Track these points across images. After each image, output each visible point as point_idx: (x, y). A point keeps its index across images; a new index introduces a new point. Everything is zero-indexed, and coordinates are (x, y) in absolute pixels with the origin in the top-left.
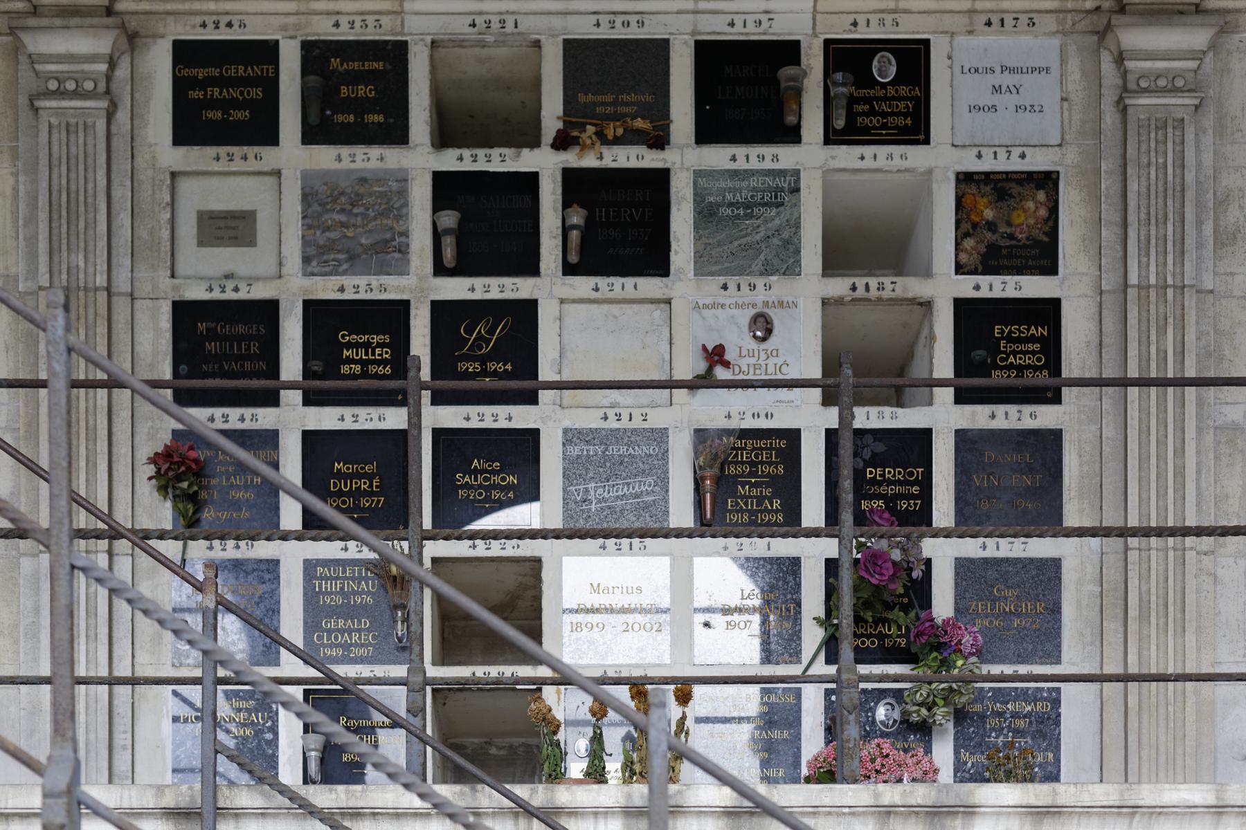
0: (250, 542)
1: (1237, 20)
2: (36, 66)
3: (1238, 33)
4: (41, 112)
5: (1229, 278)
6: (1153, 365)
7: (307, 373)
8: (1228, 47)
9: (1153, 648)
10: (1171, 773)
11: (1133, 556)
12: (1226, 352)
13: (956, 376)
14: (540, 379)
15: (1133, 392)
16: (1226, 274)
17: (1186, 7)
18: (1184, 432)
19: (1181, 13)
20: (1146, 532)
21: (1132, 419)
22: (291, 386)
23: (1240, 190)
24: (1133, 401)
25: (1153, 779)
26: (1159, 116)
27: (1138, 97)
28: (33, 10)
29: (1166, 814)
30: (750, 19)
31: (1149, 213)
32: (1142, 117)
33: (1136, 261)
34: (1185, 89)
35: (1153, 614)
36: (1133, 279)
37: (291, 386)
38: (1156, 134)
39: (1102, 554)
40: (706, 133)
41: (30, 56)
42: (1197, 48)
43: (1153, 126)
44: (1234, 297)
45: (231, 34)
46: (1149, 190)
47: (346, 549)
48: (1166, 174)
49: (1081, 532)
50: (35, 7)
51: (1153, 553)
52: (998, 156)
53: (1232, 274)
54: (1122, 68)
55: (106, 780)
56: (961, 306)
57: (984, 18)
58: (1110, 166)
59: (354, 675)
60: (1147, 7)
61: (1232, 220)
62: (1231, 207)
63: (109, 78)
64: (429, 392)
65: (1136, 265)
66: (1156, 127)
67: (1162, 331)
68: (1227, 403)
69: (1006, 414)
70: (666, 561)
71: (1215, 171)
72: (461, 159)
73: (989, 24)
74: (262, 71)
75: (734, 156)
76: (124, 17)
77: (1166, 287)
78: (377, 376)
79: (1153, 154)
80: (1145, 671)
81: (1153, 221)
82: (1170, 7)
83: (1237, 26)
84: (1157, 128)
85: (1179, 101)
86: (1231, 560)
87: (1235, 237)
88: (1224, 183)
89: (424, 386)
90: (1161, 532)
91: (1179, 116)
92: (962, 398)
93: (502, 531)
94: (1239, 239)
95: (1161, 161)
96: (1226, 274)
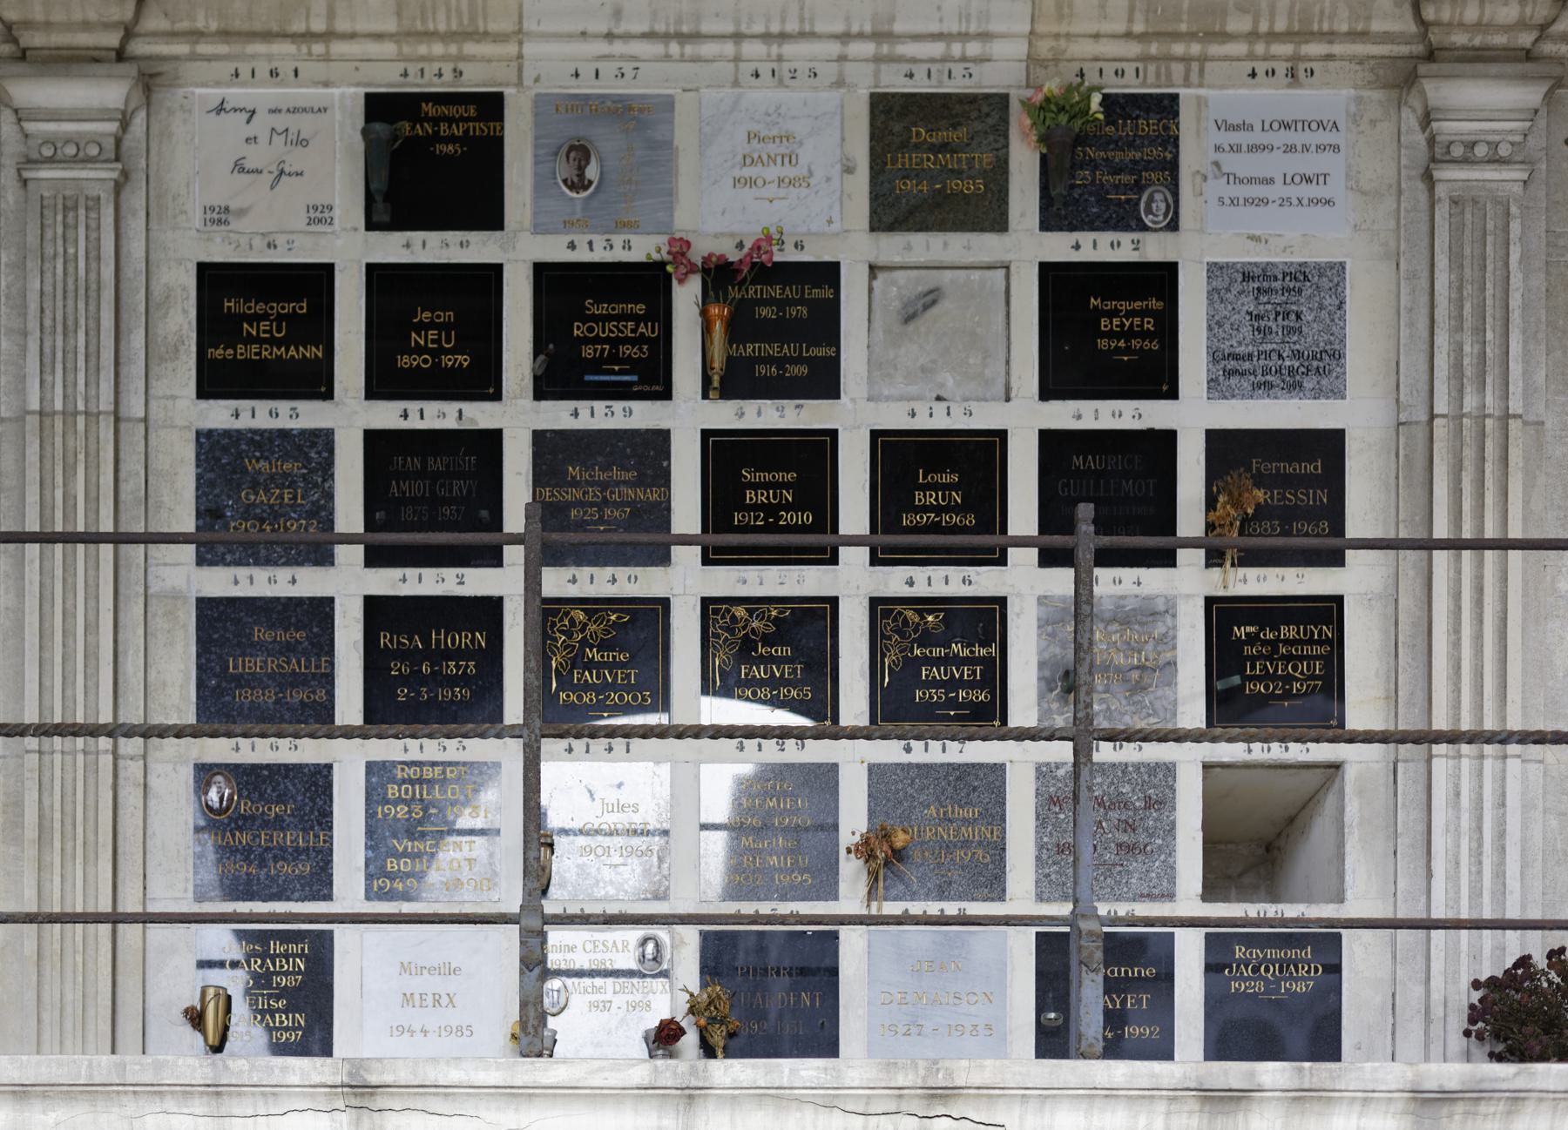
0: (1266, 745)
3: (180, 86)
4: (29, 183)
5: (170, 403)
6: (59, 515)
11: (1440, 767)
12: (165, 499)
13: (1041, 532)
14: (841, 532)
15: (1440, 557)
17: (104, 53)
19: (96, 60)
20: (1453, 738)
21: (31, 583)
22: (686, 540)
23: (184, 289)
24: (32, 561)
25: (57, 1048)
26: (68, 193)
27: (38, 169)
28: (19, 55)
29: (1117, 1096)
30: (1109, 69)
31: (54, 319)
32: (46, 194)
34: (102, 158)
36: (1441, 407)
37: (686, 540)
38: (65, 217)
39: (144, 757)
40: (490, 217)
41: (16, 111)
42: (112, 106)
43: (60, 206)
44: (175, 427)
47: (1250, 751)
48: (76, 268)
49: (1368, 737)
50: (24, 51)
53: (174, 398)
55: (34, 1048)
57: (751, 67)
58: (13, 257)
59: (768, 912)
60: (54, 52)
62: (172, 311)
63: (118, 142)
65: (37, 386)
68: (165, 564)
70: (665, 770)
71: (24, 264)
72: (909, 247)
73: (1253, 75)
74: (489, 128)
75: (572, 242)
77: (76, 413)
78: (789, 529)
79: (60, 242)
81: (59, 329)
83: (177, 78)
84: (65, 208)
85: (92, 174)
86: (169, 767)
87: (177, 350)
88: (163, 281)
90: (1474, 738)
92: (376, 557)
93: (1376, 733)
94: (182, 352)
95: (71, 251)
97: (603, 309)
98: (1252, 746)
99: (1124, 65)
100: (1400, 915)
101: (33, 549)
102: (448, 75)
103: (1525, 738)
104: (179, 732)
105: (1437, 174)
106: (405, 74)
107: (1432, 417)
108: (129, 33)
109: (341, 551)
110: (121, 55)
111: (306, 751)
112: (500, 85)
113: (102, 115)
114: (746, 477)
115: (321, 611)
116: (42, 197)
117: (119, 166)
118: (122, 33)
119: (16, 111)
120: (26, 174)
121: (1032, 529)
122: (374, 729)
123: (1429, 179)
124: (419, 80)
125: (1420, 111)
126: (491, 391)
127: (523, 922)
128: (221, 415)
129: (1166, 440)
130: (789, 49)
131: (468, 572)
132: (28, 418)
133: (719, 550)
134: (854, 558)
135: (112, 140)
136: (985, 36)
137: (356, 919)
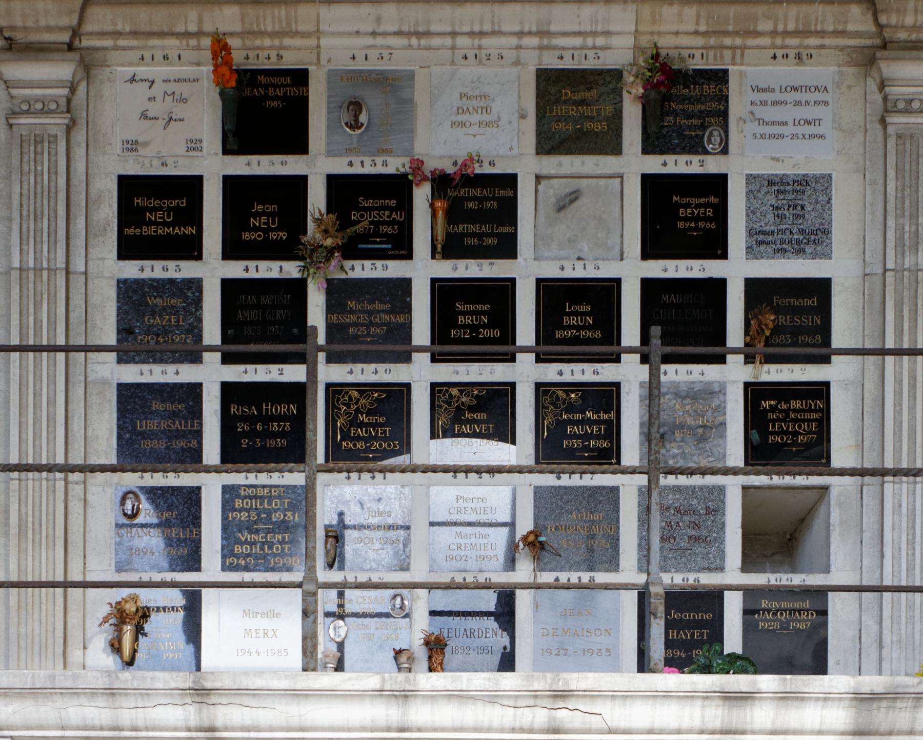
1: (105, 55)
2: (10, 90)
5: (100, 262)
7: (225, 339)
8: (101, 77)
9: (30, 559)
10: (37, 659)
12: (98, 322)
15: (889, 359)
16: (99, 259)
18: (55, 386)
21: (14, 375)
24: (15, 361)
26: (37, 132)
28: (8, 47)
31: (29, 211)
32: (24, 133)
33: (18, 249)
34: (58, 111)
35: (30, 532)
36: (890, 265)
38: (35, 147)
41: (5, 82)
43: (32, 141)
44: (105, 277)
45: (562, 65)
46: (29, 191)
49: (842, 472)
51: (30, 483)
52: (365, 164)
53: (103, 259)
54: (883, 92)
56: (227, 284)
61: (103, 216)
63: (69, 101)
64: (324, 354)
66: (35, 141)
67: (37, 305)
68: (98, 363)
69: (363, 370)
73: (775, 57)
76: (83, 52)
79: (32, 163)
80: (23, 579)
81: (32, 217)
82: (47, 45)
85: (52, 121)
89: (320, 349)
90: (39, 468)
91: (53, 132)
92: (228, 359)
96: (99, 259)
97: (370, 203)
98: (144, 474)
99: (694, 51)
100: (865, 583)
101: (15, 356)
102: (274, 58)
103: (896, 472)
104: (103, 469)
105: (889, 120)
106: (247, 58)
107: (885, 270)
108: (76, 33)
109: (206, 356)
110: (70, 47)
111: (186, 480)
112: (306, 64)
113: (58, 84)
114: (458, 308)
115: (194, 391)
116: (21, 135)
117: (69, 115)
118: (71, 33)
119: (5, 82)
120: (11, 121)
121: (217, 341)
122: (539, 467)
123: (883, 122)
124: (256, 62)
125: (878, 80)
126: (719, 252)
127: (304, 587)
128: (132, 269)
129: (721, 284)
130: (486, 42)
131: (598, 366)
132: (12, 272)
133: (126, 352)
134: (526, 360)
135: (65, 100)
136: (607, 33)
137: (225, 585)
